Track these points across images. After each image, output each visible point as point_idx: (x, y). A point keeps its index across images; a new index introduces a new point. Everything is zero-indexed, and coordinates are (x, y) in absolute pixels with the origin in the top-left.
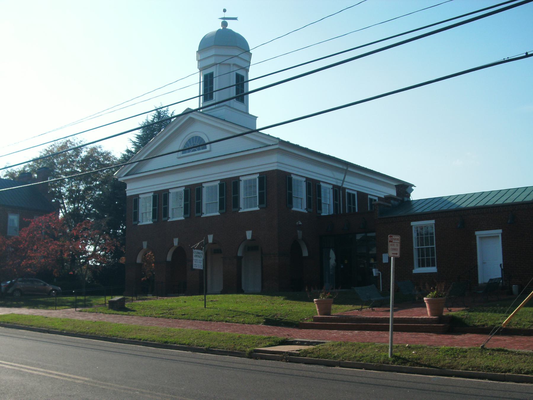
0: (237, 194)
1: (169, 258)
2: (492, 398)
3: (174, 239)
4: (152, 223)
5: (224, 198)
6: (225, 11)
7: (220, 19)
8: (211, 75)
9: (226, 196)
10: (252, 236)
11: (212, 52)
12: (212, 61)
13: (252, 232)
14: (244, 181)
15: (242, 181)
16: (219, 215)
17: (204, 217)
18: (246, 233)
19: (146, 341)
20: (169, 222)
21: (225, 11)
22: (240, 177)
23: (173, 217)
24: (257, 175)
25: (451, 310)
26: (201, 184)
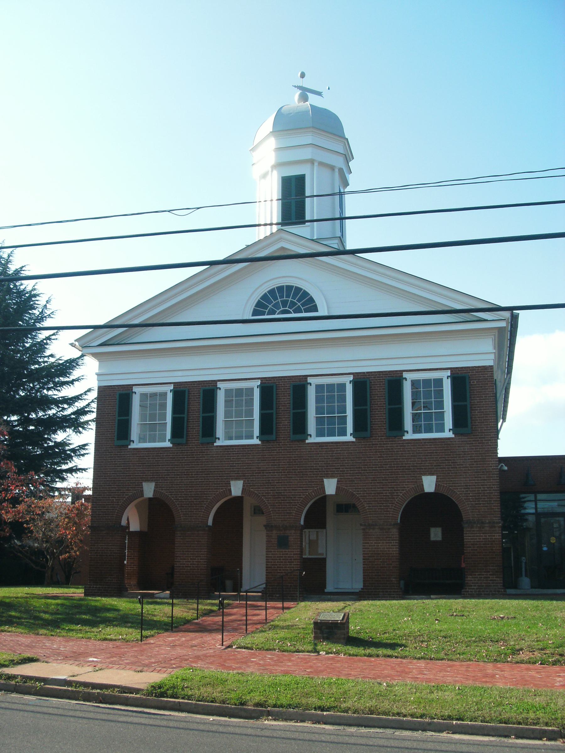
0: (128, 416)
1: (210, 523)
2: (416, 751)
3: (232, 483)
4: (171, 445)
5: (272, 413)
6: (303, 75)
7: (295, 86)
8: (300, 180)
9: (188, 415)
10: (338, 488)
11: (308, 139)
12: (307, 154)
13: (437, 479)
14: (316, 385)
15: (408, 379)
16: (353, 442)
17: (408, 440)
18: (422, 479)
19: (505, 723)
20: (217, 446)
21: (303, 75)
22: (308, 378)
23: (264, 441)
24: (255, 383)
25: (346, 618)
26: (130, 387)
